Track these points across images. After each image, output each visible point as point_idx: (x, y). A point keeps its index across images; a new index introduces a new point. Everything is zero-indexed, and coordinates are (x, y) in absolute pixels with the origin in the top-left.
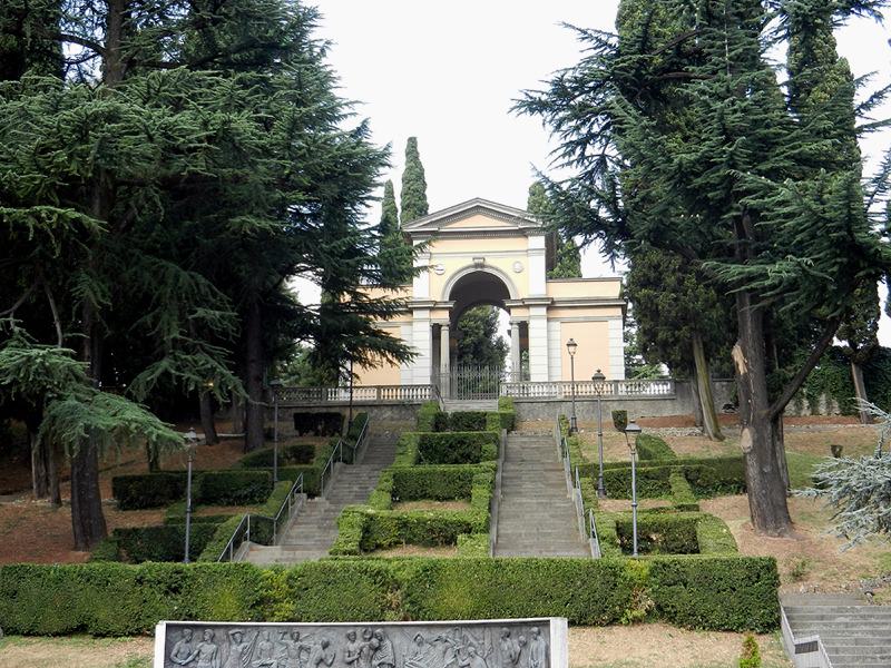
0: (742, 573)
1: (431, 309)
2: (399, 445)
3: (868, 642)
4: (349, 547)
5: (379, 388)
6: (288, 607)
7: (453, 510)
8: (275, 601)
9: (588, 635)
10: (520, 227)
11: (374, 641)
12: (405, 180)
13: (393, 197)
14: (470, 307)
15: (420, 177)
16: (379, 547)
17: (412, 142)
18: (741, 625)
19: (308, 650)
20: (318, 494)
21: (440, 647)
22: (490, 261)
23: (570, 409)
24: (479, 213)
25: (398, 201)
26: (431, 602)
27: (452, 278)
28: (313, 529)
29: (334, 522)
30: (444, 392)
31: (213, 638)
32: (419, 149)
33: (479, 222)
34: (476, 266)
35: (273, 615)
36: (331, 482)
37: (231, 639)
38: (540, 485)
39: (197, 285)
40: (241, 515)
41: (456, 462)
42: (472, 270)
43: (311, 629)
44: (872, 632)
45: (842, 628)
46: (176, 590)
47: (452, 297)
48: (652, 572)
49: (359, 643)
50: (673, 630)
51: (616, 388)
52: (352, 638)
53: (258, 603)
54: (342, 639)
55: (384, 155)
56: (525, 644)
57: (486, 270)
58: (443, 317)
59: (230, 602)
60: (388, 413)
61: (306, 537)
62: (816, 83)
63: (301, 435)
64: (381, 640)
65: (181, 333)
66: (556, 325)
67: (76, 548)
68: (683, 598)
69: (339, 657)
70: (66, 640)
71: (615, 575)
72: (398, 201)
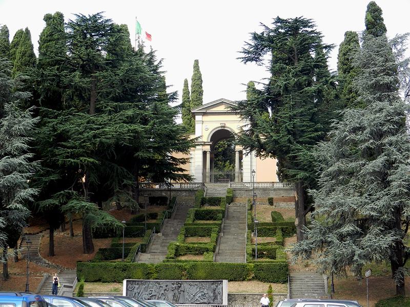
0: (278, 268)
2: (188, 214)
3: (310, 286)
4: (171, 256)
6: (156, 275)
7: (206, 241)
8: (152, 273)
11: (179, 285)
13: (188, 87)
14: (218, 141)
16: (181, 255)
17: (197, 62)
18: (278, 281)
19: (162, 287)
20: (160, 232)
21: (196, 287)
22: (227, 125)
23: (257, 194)
25: (190, 88)
26: (195, 274)
28: (158, 246)
31: (138, 284)
32: (199, 65)
33: (222, 108)
34: (222, 127)
35: (151, 277)
36: (164, 226)
38: (237, 229)
39: (124, 172)
40: (138, 242)
41: (208, 220)
42: (220, 128)
44: (313, 284)
45: (305, 282)
46: (125, 270)
48: (254, 267)
49: (175, 285)
50: (260, 282)
51: (273, 185)
52: (173, 284)
53: (148, 274)
54: (171, 284)
56: (217, 286)
57: (226, 129)
59: (140, 273)
60: (184, 194)
61: (157, 249)
63: (151, 205)
65: (119, 189)
67: (84, 253)
68: (262, 274)
69: (170, 289)
70: (95, 283)
71: (244, 267)
72: (190, 88)
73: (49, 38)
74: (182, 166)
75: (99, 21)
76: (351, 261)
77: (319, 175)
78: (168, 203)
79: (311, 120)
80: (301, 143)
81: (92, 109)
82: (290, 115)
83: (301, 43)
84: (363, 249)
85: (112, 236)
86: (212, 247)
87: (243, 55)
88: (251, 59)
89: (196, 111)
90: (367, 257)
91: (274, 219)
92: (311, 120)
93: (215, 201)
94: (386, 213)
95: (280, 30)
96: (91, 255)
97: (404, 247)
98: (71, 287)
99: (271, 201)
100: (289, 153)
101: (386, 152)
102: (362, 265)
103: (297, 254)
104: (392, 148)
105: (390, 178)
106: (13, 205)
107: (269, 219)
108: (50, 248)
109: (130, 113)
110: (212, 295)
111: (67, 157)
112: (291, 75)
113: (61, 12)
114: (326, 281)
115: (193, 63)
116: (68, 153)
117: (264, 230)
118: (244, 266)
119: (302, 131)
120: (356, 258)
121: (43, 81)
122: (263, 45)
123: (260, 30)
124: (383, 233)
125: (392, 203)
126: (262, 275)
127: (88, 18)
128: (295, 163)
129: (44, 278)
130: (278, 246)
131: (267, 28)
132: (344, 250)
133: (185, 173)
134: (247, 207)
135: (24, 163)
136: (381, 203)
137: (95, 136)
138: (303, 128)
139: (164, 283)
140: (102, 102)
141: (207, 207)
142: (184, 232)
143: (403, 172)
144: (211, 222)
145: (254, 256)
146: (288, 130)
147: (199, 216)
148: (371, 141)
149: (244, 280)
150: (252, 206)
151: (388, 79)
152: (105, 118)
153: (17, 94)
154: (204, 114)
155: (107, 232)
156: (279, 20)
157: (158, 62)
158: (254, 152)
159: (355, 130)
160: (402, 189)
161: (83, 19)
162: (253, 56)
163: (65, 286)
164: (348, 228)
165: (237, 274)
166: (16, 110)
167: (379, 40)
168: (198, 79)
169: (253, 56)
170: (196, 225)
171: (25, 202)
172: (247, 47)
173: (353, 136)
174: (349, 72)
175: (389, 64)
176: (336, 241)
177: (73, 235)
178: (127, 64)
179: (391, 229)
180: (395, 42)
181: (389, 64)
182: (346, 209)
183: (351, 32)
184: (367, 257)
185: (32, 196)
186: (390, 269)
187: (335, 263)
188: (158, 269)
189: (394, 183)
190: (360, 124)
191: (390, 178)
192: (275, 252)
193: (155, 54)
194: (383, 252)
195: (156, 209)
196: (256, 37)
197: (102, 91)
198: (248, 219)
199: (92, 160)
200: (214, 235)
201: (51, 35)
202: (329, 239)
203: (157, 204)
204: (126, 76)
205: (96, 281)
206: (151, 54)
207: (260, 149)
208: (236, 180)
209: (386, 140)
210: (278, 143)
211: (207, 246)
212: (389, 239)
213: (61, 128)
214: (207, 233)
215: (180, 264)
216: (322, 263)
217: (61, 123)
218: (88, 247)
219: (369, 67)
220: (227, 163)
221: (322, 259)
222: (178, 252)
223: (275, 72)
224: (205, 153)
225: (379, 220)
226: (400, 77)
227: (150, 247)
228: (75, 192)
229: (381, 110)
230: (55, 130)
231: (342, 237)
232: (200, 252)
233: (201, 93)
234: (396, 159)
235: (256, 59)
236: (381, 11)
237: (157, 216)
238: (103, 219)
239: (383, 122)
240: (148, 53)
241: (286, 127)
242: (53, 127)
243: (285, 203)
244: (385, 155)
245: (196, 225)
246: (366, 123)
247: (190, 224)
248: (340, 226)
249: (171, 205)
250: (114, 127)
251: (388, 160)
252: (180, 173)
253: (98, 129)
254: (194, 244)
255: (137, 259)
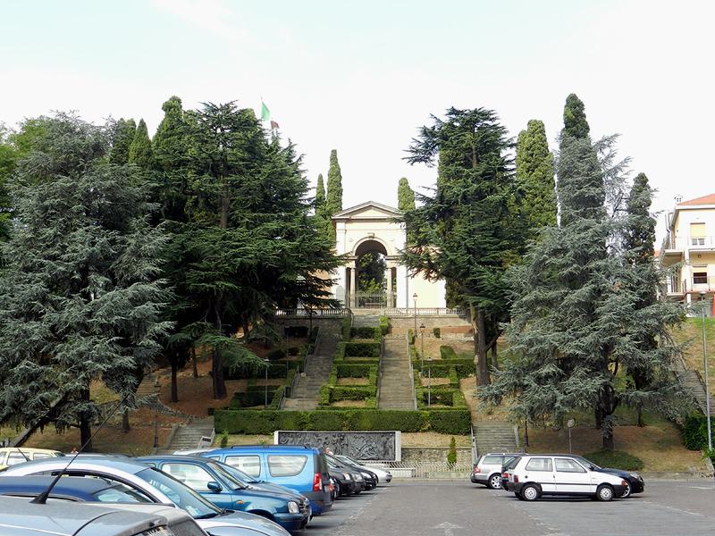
9: (409, 436)
12: (330, 175)
15: (338, 173)
17: (334, 152)
23: (423, 325)
25: (326, 187)
29: (318, 391)
30: (352, 304)
34: (370, 237)
37: (297, 437)
41: (361, 356)
52: (334, 436)
58: (352, 265)
62: (537, 166)
67: (215, 398)
68: (440, 424)
72: (326, 187)
73: (169, 132)
74: (327, 289)
75: (233, 112)
76: (551, 407)
77: (510, 304)
78: (309, 334)
79: (494, 235)
80: (483, 264)
81: (223, 221)
82: (470, 230)
83: (480, 141)
84: (565, 394)
85: (247, 377)
86: (374, 391)
87: (411, 155)
88: (420, 160)
89: (337, 217)
90: (571, 403)
91: (444, 355)
92: (494, 235)
93: (368, 332)
94: (593, 351)
95: (455, 124)
96: (225, 400)
97: (613, 391)
98: (209, 440)
99: (437, 333)
100: (469, 276)
101: (593, 280)
102: (565, 413)
103: (485, 400)
104: (601, 275)
105: (597, 311)
106: (146, 341)
107: (437, 355)
108: (173, 392)
109: (273, 225)
110: (382, 449)
111: (200, 281)
112: (470, 180)
113: (178, 95)
114: (516, 432)
115: (329, 154)
116: (202, 276)
117: (435, 369)
118: (417, 415)
119: (484, 249)
120: (557, 405)
121: (167, 186)
122: (434, 142)
123: (430, 124)
124: (590, 375)
125: (601, 340)
126: (440, 425)
127: (219, 107)
128: (475, 288)
129: (173, 430)
130: (454, 390)
131: (439, 121)
132: (543, 395)
133: (330, 297)
134: (408, 341)
135: (156, 290)
136: (589, 339)
137: (235, 256)
138: (485, 246)
139: (323, 435)
140: (237, 212)
141: (357, 340)
142: (336, 372)
143: (614, 303)
144: (366, 359)
145: (426, 402)
146: (468, 249)
147: (351, 351)
148: (575, 266)
149: (417, 431)
150: (413, 339)
151: (593, 191)
152: (242, 232)
153: (145, 205)
154: (348, 221)
155: (247, 372)
156: (453, 111)
157: (297, 158)
158: (422, 273)
159: (555, 253)
160: (612, 323)
161: (214, 109)
162: (421, 155)
163: (204, 439)
164: (548, 369)
165: (411, 424)
166: (146, 226)
167: (581, 143)
168: (336, 174)
169: (421, 155)
170: (349, 362)
171: (158, 337)
172: (414, 145)
173: (553, 260)
174: (533, 171)
175: (594, 174)
176: (534, 385)
177: (196, 375)
178: (270, 165)
179: (597, 370)
180: (601, 145)
181: (594, 174)
182: (547, 347)
183: (536, 121)
184: (571, 403)
185: (168, 330)
186: (593, 418)
187: (532, 411)
188: (314, 418)
189: (604, 318)
190: (561, 245)
191: (597, 311)
192: (451, 397)
193: (295, 149)
194: (590, 398)
195: (294, 343)
196: (425, 132)
197: (237, 198)
198: (412, 355)
199: (230, 285)
200: (373, 375)
201: (173, 128)
202: (526, 383)
203: (295, 336)
204: (268, 181)
205: (238, 433)
206: (290, 149)
207: (430, 268)
208: (389, 304)
209: (593, 265)
210: (455, 264)
211: (368, 390)
212: (598, 382)
213: (191, 246)
214: (363, 373)
215: (340, 412)
216: (515, 410)
217: (189, 239)
218: (220, 392)
219: (571, 177)
220: (372, 282)
221: (516, 405)
222: (333, 397)
223: (446, 175)
224: (348, 270)
225: (584, 359)
226: (606, 187)
227: (295, 391)
228: (209, 324)
229: (587, 228)
230: (183, 247)
231: (539, 380)
232: (360, 396)
233: (340, 193)
234: (604, 287)
235: (425, 160)
236: (583, 105)
237: (297, 352)
238: (243, 357)
239: (588, 243)
240: (285, 147)
241: (465, 244)
242: (182, 244)
243: (454, 335)
244: (592, 283)
245: (349, 362)
246: (569, 245)
247: (340, 362)
248: (538, 367)
249: (312, 338)
250: (259, 243)
251: (594, 289)
252: (324, 297)
253: (237, 247)
254: (350, 386)
255: (282, 406)
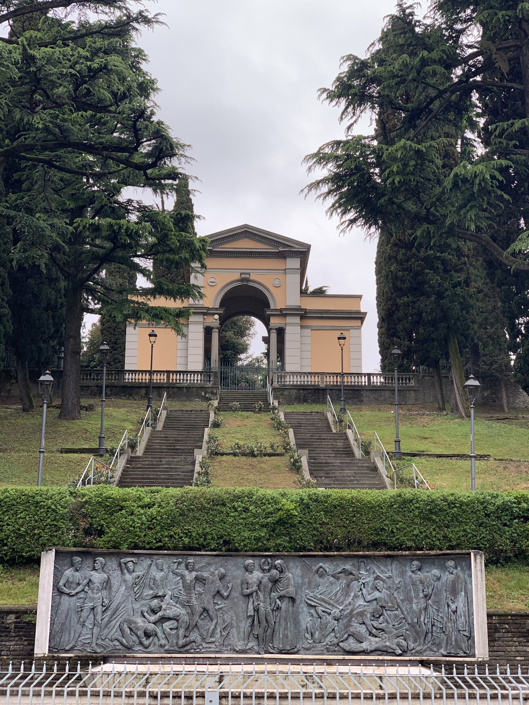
1: (204, 314)
5: (168, 372)
10: (281, 249)
22: (253, 277)
24: (246, 237)
27: (222, 289)
34: (242, 280)
43: (206, 559)
47: (222, 304)
55: (404, 11)
57: (251, 284)
58: (214, 321)
64: (281, 572)
66: (308, 332)
